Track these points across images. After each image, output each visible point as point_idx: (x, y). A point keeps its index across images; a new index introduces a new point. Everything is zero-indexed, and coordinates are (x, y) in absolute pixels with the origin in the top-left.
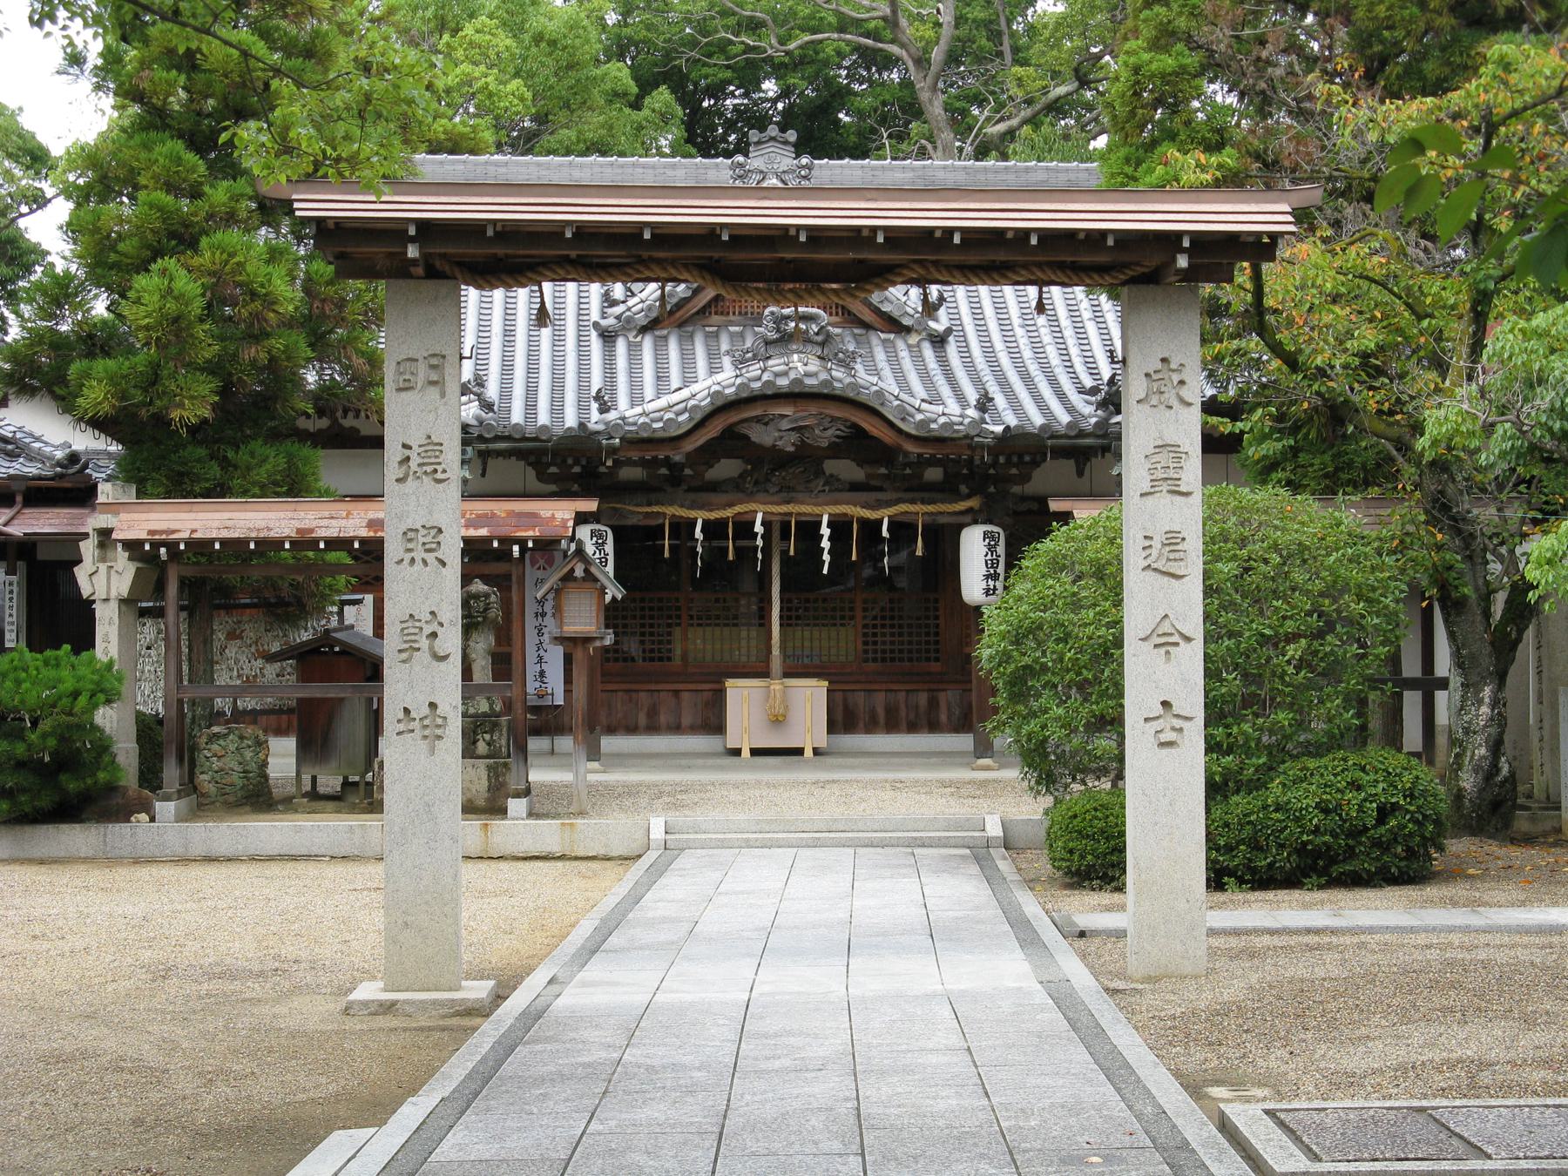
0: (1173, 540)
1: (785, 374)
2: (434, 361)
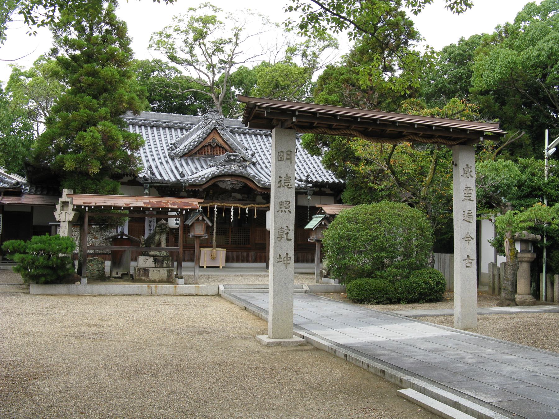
0: (470, 212)
1: (230, 170)
2: (289, 153)
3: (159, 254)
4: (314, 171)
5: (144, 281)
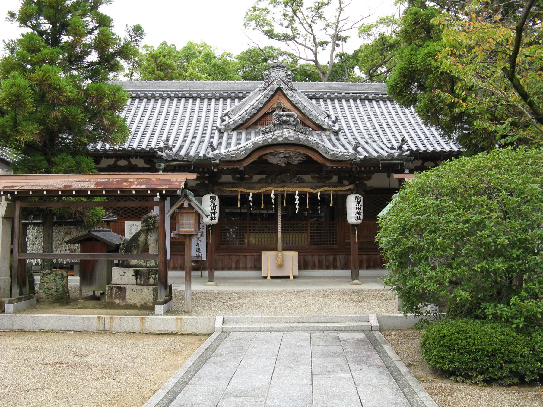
1: (281, 136)
3: (144, 264)
4: (423, 138)
5: (118, 307)
